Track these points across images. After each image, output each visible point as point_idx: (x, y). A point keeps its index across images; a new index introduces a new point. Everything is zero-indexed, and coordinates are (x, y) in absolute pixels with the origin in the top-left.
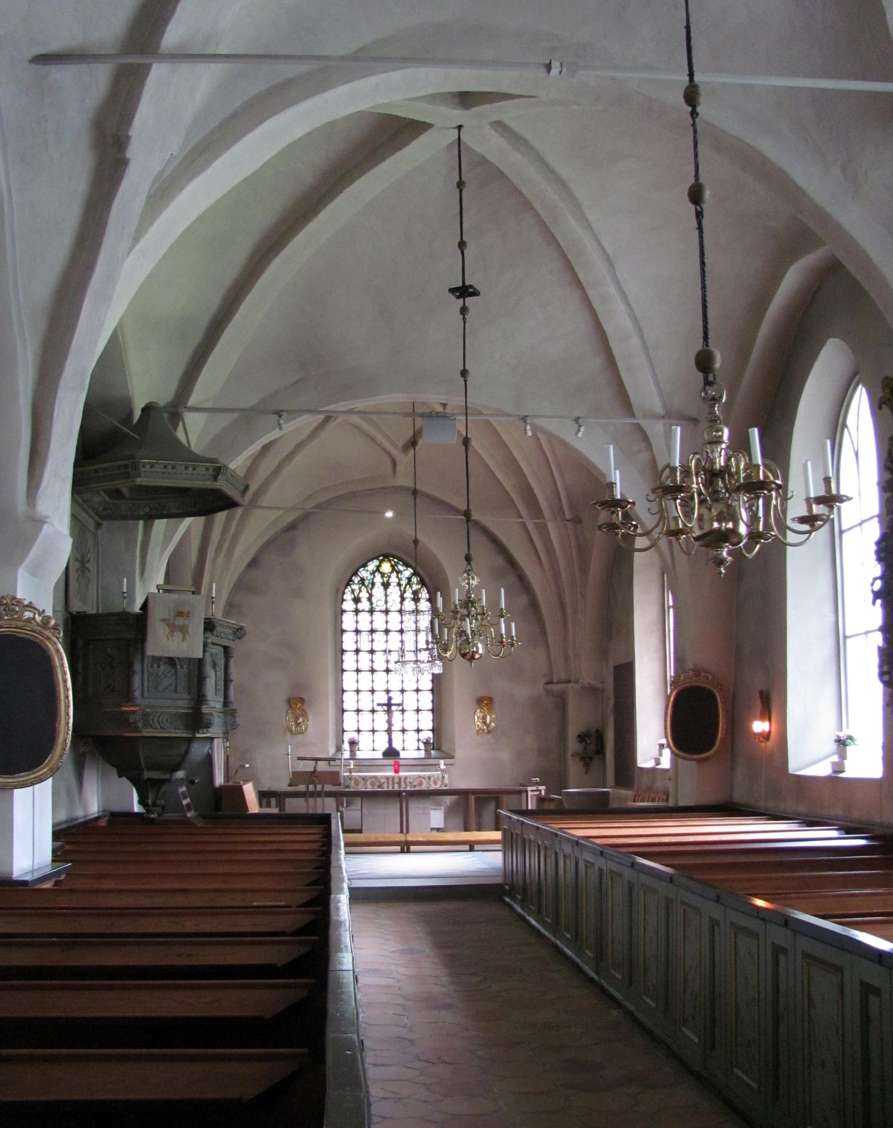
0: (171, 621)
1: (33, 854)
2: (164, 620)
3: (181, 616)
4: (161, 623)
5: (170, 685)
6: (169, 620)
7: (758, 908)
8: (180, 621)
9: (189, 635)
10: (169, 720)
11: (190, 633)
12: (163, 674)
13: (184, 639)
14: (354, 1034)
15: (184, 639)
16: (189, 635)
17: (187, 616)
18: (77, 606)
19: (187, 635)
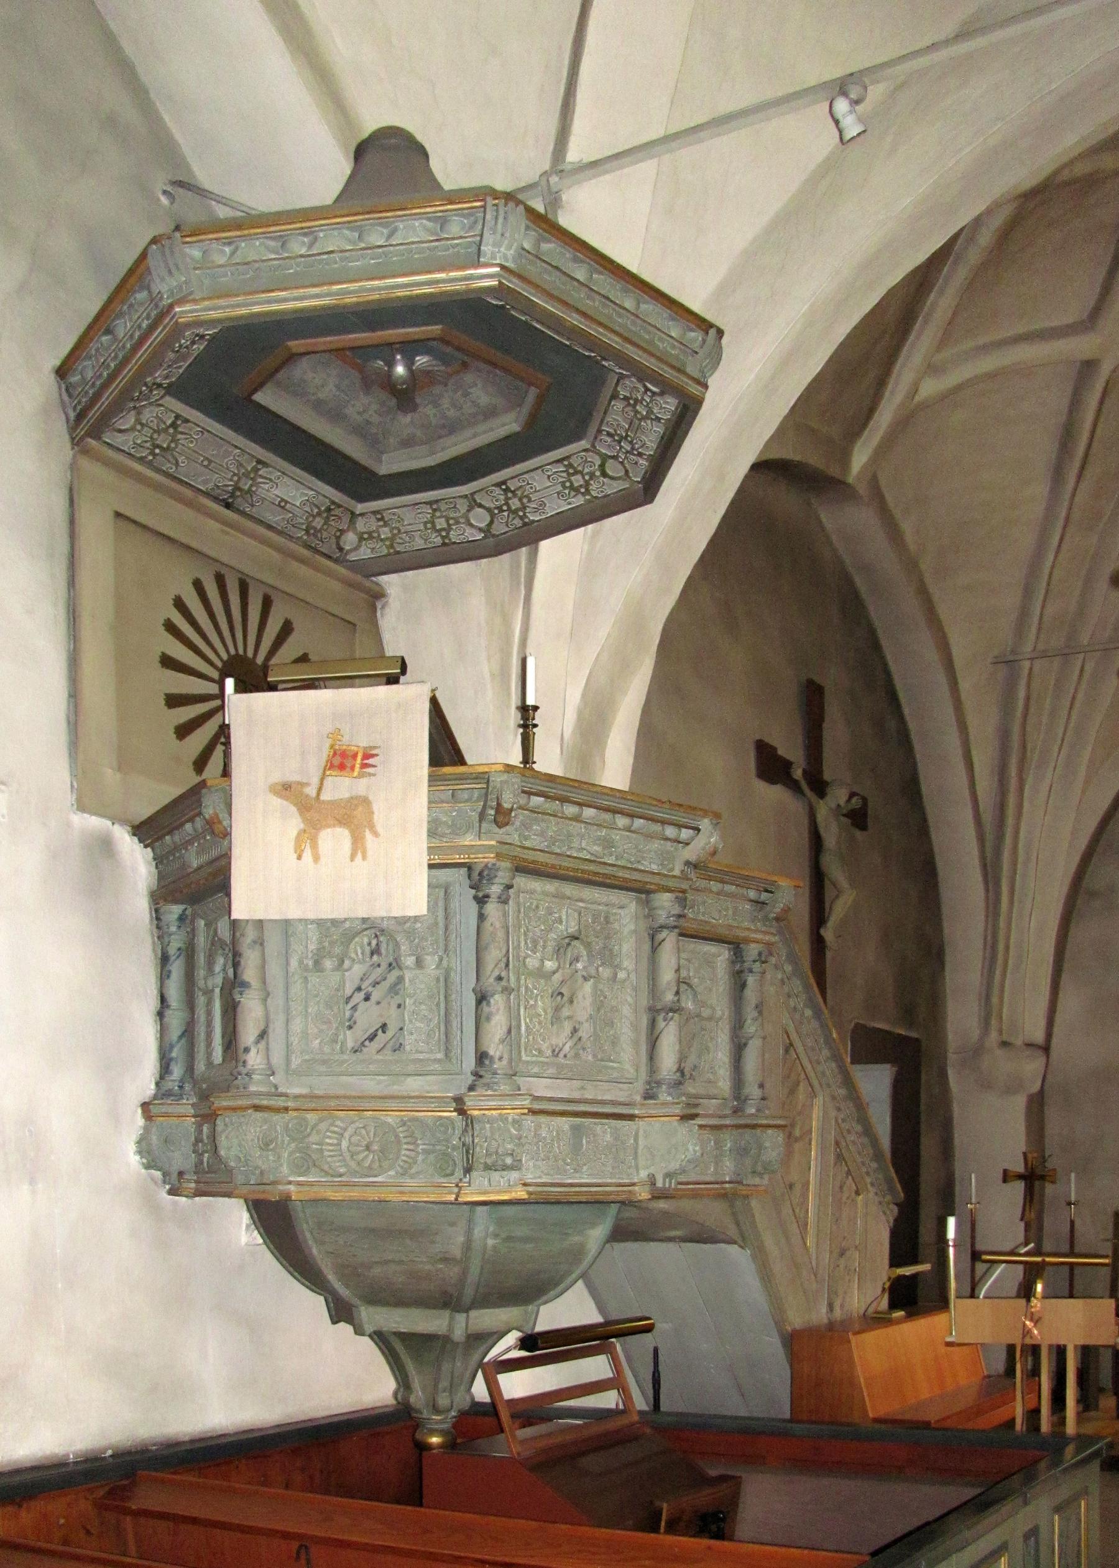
0: (311, 791)
1: (73, 535)
2: (286, 790)
3: (342, 767)
4: (277, 802)
5: (384, 1027)
6: (303, 785)
7: (838, 1033)
8: (340, 787)
9: (376, 834)
10: (375, 1147)
11: (379, 829)
12: (359, 989)
13: (358, 846)
14: (305, 1119)
15: (358, 846)
16: (376, 834)
17: (364, 766)
18: (796, 1320)
19: (368, 835)
